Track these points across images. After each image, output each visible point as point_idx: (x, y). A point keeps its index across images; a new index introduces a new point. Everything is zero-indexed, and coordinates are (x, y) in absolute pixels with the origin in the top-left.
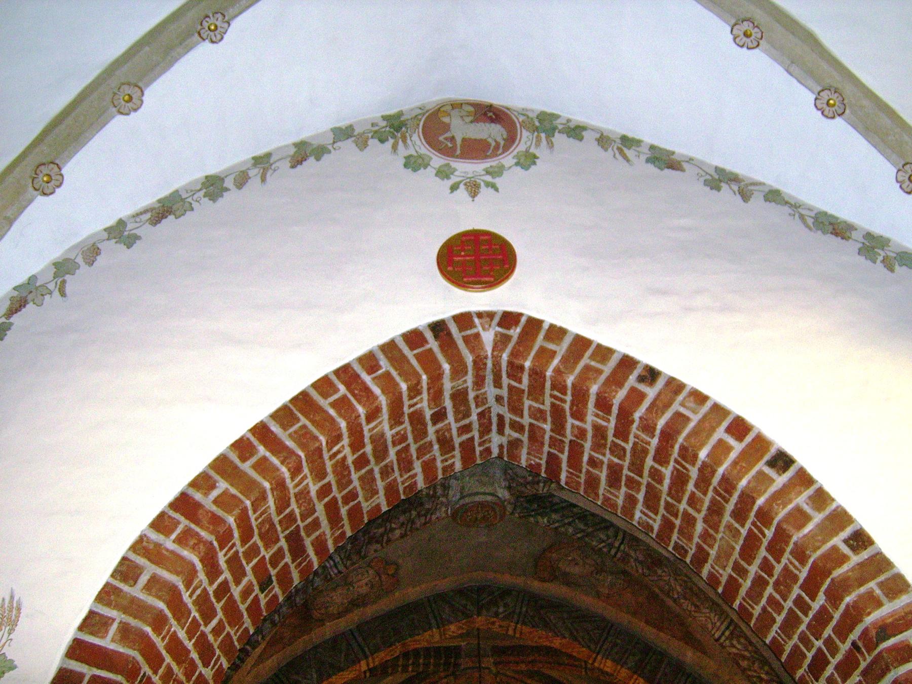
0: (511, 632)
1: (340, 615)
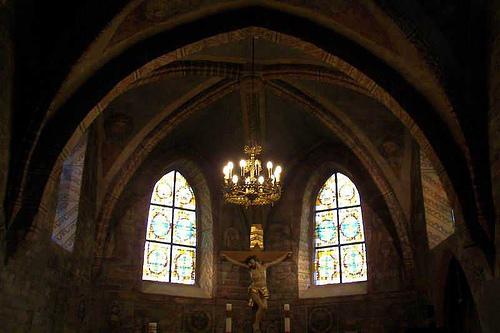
0: (274, 40)
1: (164, 19)
